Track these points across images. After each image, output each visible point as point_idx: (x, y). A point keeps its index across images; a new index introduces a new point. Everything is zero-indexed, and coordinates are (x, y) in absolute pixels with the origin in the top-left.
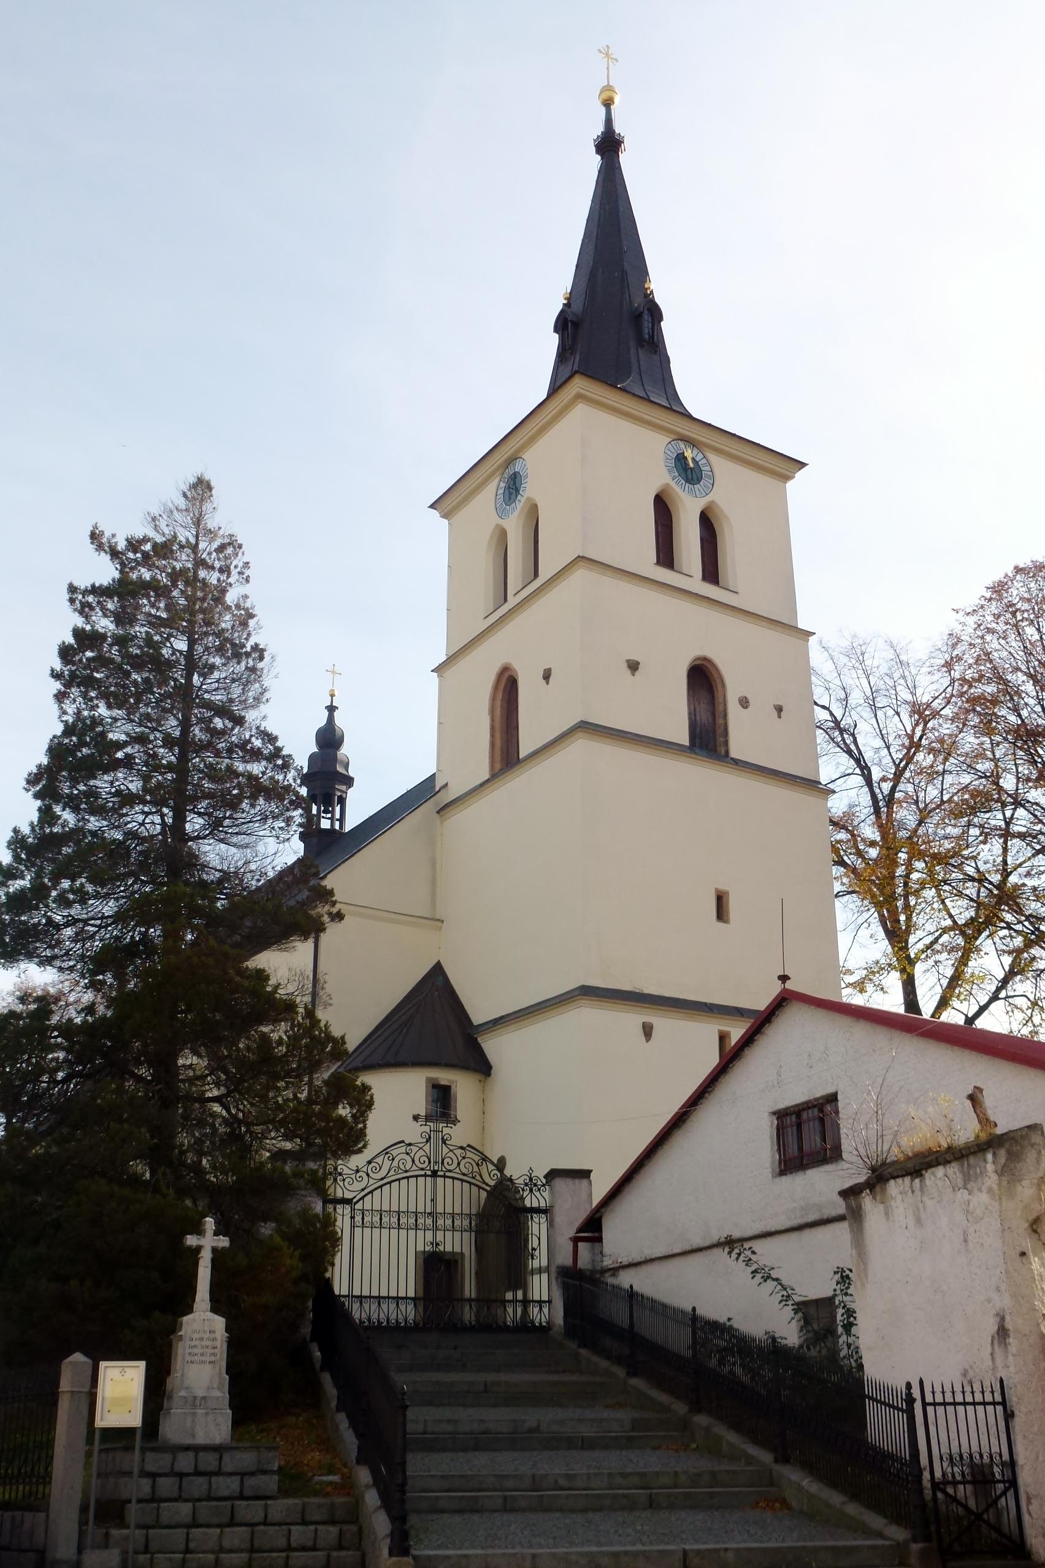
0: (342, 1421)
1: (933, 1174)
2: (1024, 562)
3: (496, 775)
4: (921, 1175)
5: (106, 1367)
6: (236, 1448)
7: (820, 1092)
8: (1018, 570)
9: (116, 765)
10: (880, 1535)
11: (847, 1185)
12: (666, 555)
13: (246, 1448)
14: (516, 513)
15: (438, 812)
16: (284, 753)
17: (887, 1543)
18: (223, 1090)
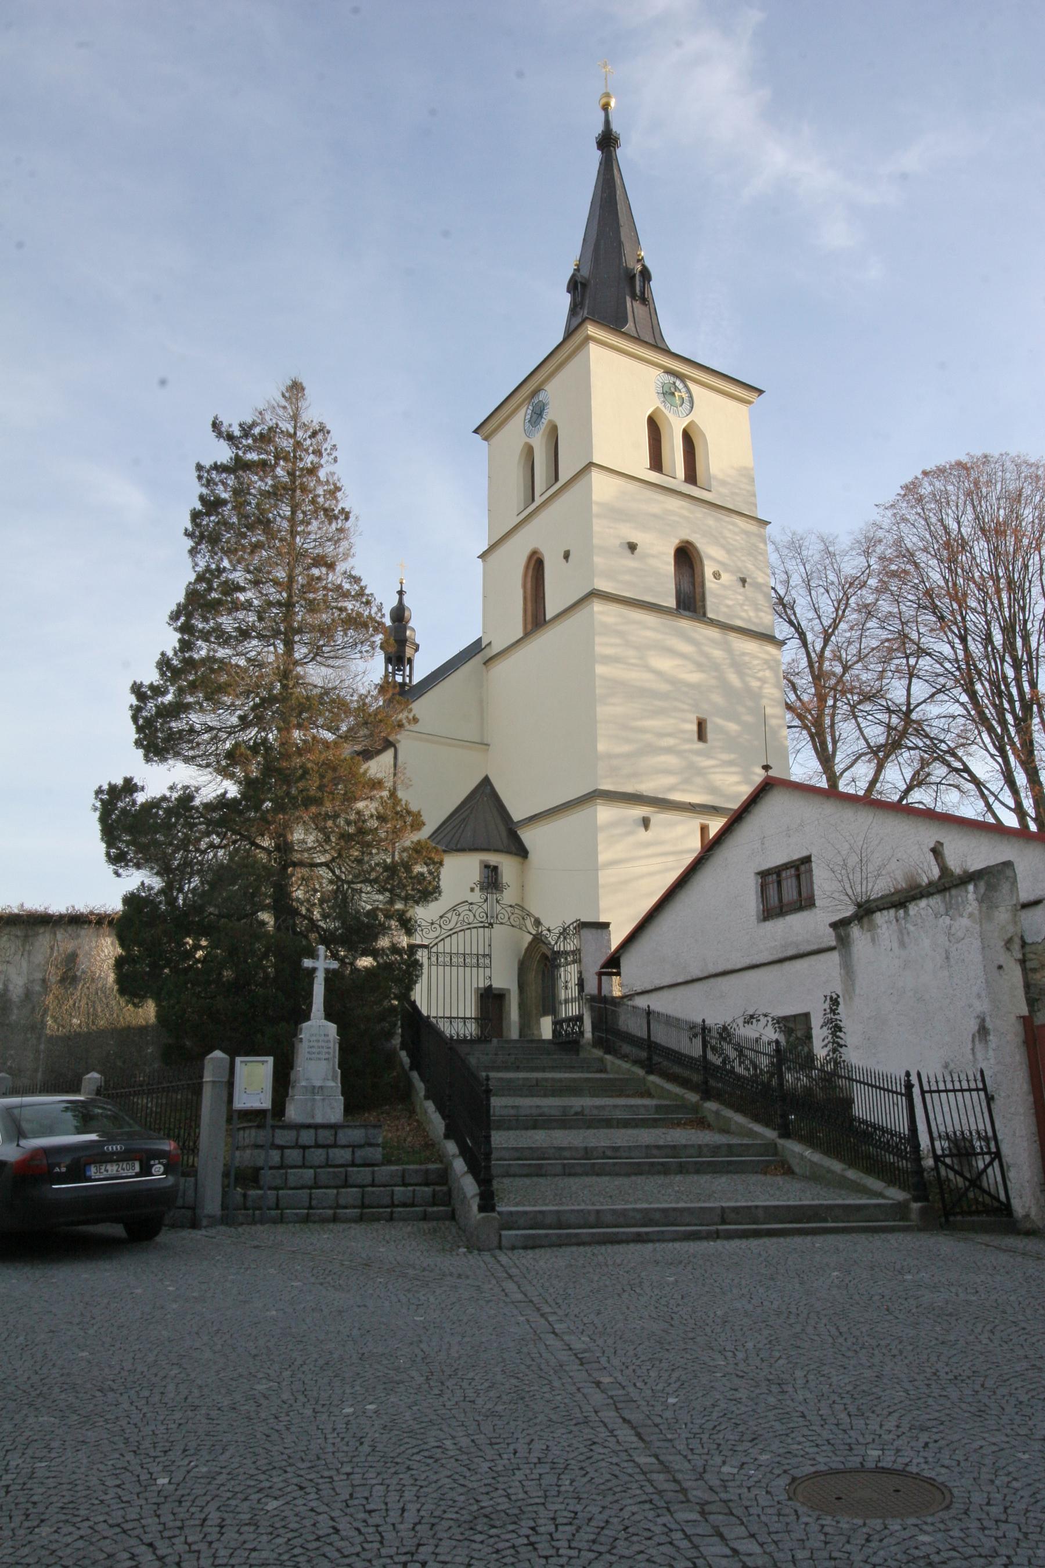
0: (430, 1106)
1: (917, 905)
2: (930, 467)
3: (527, 634)
4: (905, 907)
5: (242, 1062)
6: (348, 1126)
7: (796, 856)
8: (925, 473)
9: (236, 606)
10: (881, 1195)
11: (836, 918)
12: (657, 463)
13: (355, 1126)
14: (541, 432)
15: (485, 664)
16: (367, 592)
17: (891, 1202)
18: (328, 857)
